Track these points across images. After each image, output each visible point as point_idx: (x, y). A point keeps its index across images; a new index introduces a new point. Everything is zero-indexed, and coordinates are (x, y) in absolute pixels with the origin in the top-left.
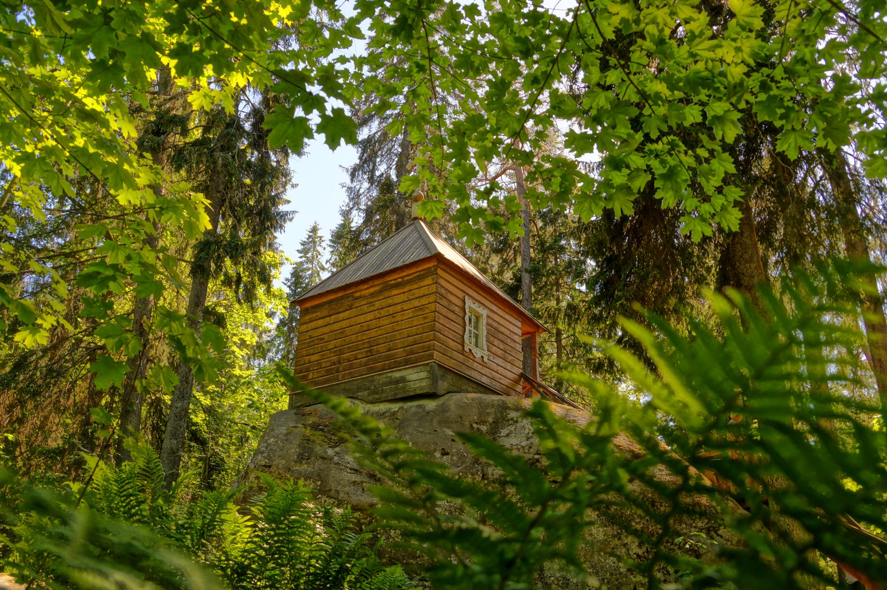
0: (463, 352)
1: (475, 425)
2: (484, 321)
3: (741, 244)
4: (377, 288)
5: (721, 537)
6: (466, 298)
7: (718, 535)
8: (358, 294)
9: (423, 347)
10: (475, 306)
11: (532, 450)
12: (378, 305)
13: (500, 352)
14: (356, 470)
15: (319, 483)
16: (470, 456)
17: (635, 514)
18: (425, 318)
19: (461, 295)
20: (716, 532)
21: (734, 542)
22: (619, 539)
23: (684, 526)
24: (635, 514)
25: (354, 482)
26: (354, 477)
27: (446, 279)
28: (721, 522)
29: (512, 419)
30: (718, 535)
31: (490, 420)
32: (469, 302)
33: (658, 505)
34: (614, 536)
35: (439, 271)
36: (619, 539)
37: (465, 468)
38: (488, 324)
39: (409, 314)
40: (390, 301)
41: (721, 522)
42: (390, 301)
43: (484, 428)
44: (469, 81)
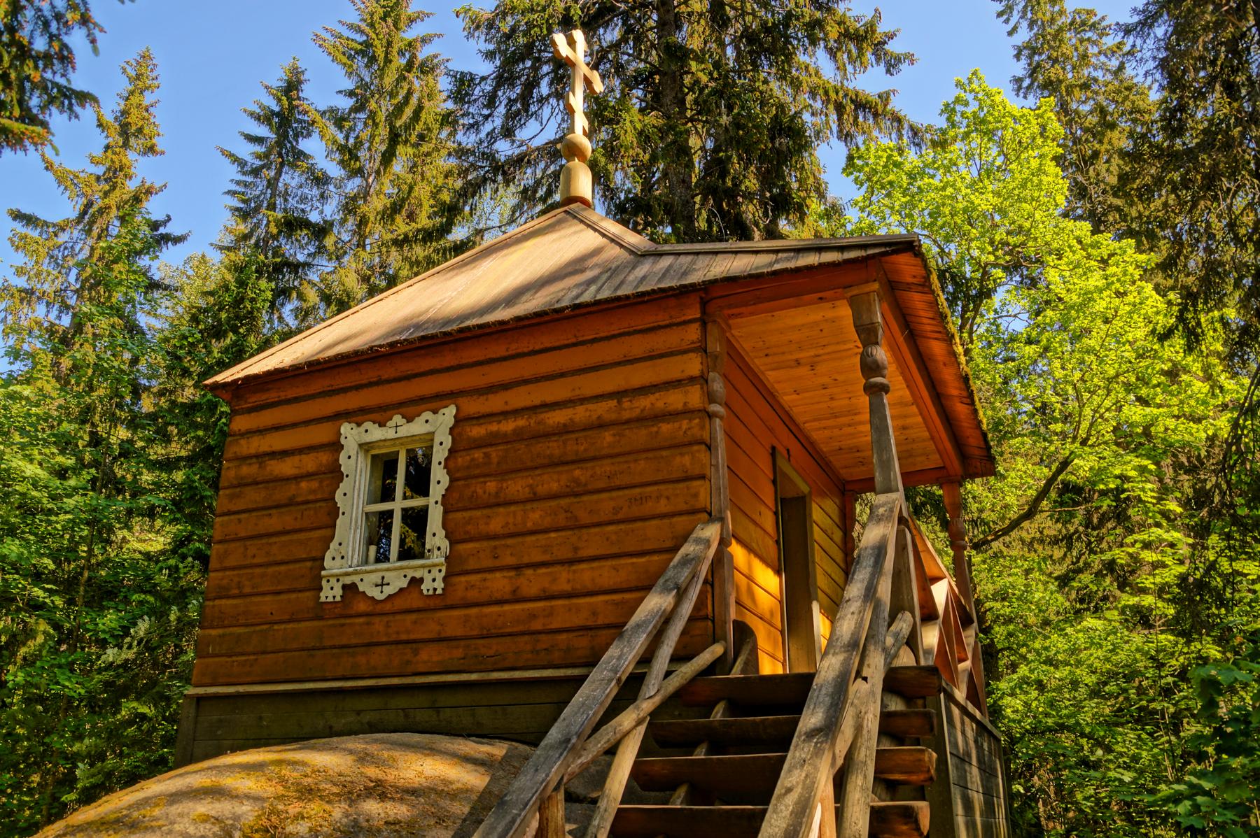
13: (536, 516)
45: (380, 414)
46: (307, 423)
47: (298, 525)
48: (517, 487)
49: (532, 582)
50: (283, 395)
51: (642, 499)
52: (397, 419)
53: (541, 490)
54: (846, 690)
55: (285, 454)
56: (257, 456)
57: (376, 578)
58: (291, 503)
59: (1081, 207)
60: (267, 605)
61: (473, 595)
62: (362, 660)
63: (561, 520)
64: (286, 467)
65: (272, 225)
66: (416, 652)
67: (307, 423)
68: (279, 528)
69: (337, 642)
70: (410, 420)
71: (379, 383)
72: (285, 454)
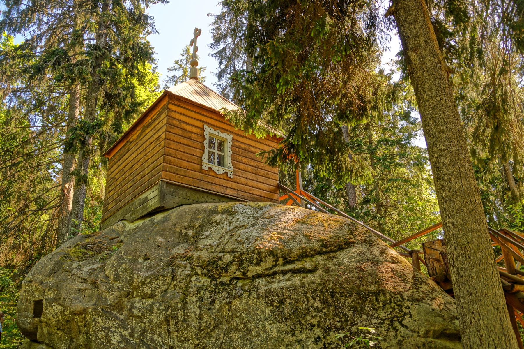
0: (201, 171)
1: (184, 231)
2: (228, 145)
3: (404, 8)
4: (140, 131)
5: (407, 327)
6: (206, 126)
7: (403, 325)
8: (131, 140)
9: (157, 170)
10: (218, 133)
11: (218, 249)
12: (139, 144)
13: (249, 168)
14: (85, 280)
15: (56, 292)
16: (166, 259)
17: (312, 306)
18: (160, 146)
19: (199, 124)
20: (400, 323)
21: (421, 333)
22: (293, 335)
23: (365, 317)
24: (312, 306)
25: (80, 290)
26: (82, 286)
27: (178, 113)
28: (406, 311)
29: (216, 222)
30: (403, 325)
31: (198, 224)
32: (208, 130)
33: (338, 295)
34: (287, 333)
35: (171, 107)
36: (293, 335)
37: (159, 270)
38: (233, 146)
39: (152, 146)
40: (145, 139)
41: (406, 311)
42: (145, 139)
43: (191, 232)
44: (329, 20)
45: (216, 127)
46: (197, 120)
47: (192, 145)
48: (245, 160)
49: (250, 183)
50: (185, 106)
51: (145, 165)
52: (219, 131)
53: (251, 164)
54: (414, 89)
55: (189, 124)
56: (181, 120)
57: (217, 168)
58: (189, 138)
59: (415, 287)
60: (185, 164)
61: (238, 181)
62: (214, 187)
63: (254, 172)
64: (188, 128)
65: (273, 131)
66: (226, 190)
67: (197, 120)
68: (187, 144)
69: (206, 180)
70: (222, 133)
71: (213, 118)
72: (189, 124)
